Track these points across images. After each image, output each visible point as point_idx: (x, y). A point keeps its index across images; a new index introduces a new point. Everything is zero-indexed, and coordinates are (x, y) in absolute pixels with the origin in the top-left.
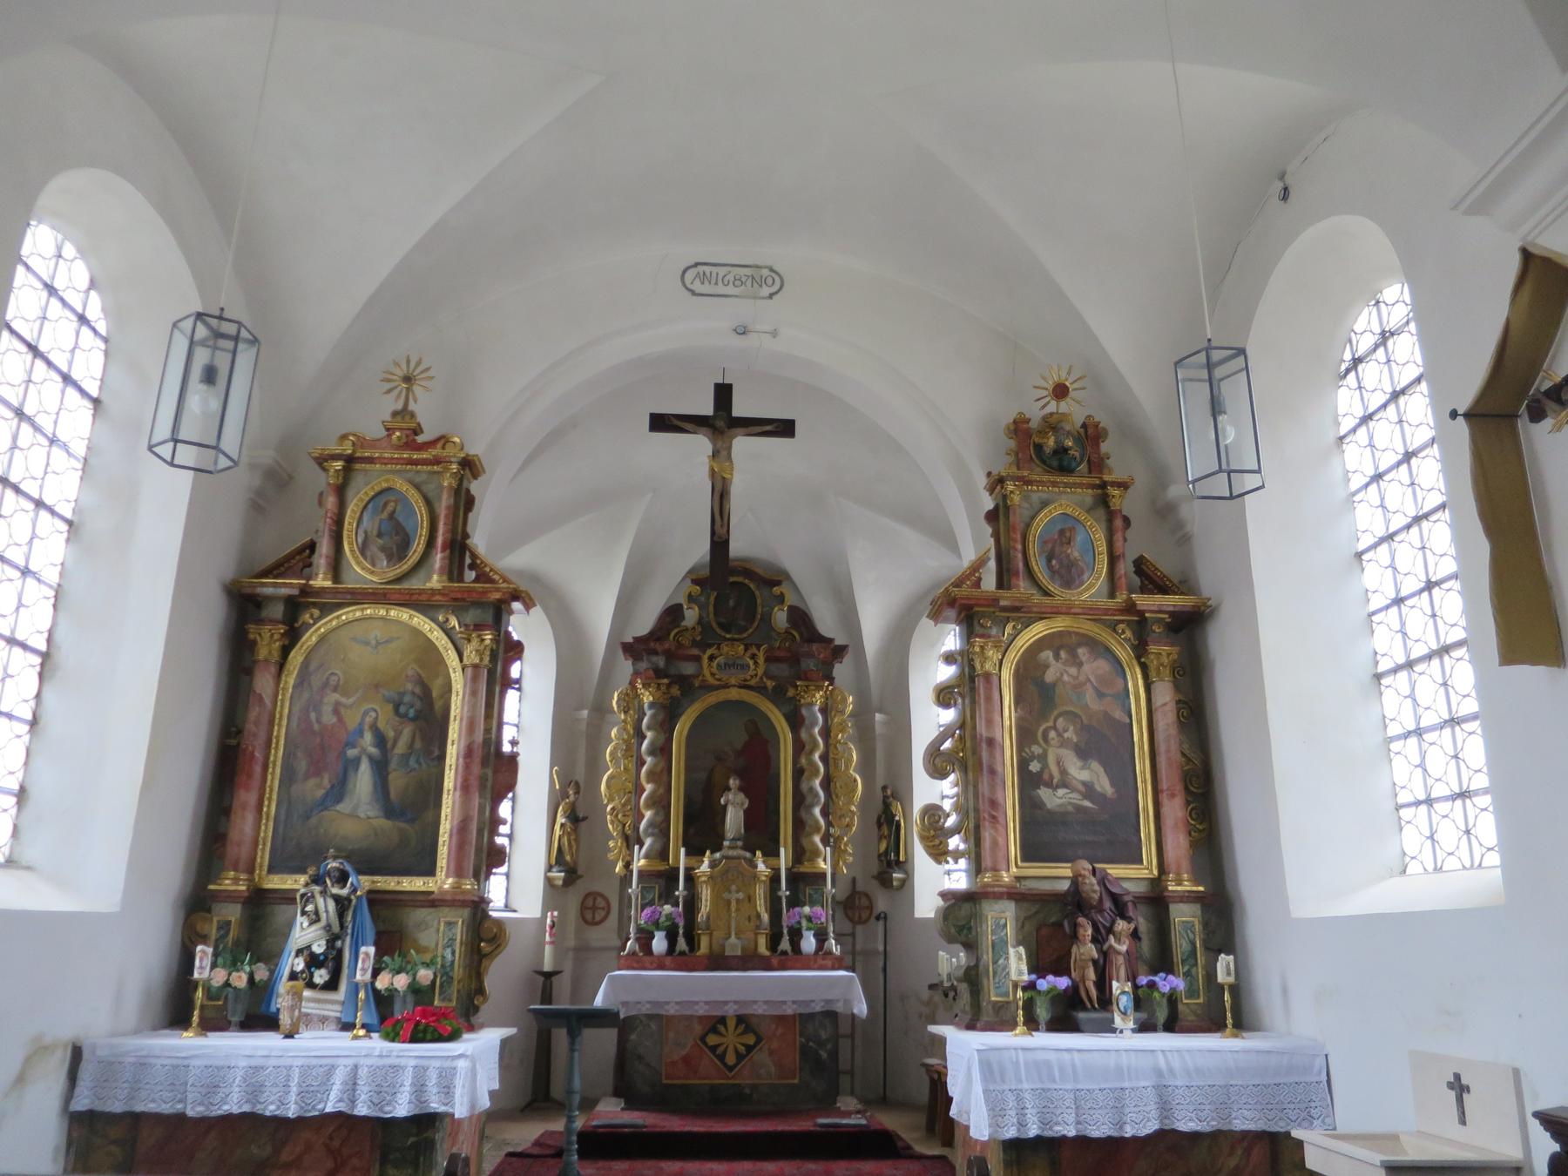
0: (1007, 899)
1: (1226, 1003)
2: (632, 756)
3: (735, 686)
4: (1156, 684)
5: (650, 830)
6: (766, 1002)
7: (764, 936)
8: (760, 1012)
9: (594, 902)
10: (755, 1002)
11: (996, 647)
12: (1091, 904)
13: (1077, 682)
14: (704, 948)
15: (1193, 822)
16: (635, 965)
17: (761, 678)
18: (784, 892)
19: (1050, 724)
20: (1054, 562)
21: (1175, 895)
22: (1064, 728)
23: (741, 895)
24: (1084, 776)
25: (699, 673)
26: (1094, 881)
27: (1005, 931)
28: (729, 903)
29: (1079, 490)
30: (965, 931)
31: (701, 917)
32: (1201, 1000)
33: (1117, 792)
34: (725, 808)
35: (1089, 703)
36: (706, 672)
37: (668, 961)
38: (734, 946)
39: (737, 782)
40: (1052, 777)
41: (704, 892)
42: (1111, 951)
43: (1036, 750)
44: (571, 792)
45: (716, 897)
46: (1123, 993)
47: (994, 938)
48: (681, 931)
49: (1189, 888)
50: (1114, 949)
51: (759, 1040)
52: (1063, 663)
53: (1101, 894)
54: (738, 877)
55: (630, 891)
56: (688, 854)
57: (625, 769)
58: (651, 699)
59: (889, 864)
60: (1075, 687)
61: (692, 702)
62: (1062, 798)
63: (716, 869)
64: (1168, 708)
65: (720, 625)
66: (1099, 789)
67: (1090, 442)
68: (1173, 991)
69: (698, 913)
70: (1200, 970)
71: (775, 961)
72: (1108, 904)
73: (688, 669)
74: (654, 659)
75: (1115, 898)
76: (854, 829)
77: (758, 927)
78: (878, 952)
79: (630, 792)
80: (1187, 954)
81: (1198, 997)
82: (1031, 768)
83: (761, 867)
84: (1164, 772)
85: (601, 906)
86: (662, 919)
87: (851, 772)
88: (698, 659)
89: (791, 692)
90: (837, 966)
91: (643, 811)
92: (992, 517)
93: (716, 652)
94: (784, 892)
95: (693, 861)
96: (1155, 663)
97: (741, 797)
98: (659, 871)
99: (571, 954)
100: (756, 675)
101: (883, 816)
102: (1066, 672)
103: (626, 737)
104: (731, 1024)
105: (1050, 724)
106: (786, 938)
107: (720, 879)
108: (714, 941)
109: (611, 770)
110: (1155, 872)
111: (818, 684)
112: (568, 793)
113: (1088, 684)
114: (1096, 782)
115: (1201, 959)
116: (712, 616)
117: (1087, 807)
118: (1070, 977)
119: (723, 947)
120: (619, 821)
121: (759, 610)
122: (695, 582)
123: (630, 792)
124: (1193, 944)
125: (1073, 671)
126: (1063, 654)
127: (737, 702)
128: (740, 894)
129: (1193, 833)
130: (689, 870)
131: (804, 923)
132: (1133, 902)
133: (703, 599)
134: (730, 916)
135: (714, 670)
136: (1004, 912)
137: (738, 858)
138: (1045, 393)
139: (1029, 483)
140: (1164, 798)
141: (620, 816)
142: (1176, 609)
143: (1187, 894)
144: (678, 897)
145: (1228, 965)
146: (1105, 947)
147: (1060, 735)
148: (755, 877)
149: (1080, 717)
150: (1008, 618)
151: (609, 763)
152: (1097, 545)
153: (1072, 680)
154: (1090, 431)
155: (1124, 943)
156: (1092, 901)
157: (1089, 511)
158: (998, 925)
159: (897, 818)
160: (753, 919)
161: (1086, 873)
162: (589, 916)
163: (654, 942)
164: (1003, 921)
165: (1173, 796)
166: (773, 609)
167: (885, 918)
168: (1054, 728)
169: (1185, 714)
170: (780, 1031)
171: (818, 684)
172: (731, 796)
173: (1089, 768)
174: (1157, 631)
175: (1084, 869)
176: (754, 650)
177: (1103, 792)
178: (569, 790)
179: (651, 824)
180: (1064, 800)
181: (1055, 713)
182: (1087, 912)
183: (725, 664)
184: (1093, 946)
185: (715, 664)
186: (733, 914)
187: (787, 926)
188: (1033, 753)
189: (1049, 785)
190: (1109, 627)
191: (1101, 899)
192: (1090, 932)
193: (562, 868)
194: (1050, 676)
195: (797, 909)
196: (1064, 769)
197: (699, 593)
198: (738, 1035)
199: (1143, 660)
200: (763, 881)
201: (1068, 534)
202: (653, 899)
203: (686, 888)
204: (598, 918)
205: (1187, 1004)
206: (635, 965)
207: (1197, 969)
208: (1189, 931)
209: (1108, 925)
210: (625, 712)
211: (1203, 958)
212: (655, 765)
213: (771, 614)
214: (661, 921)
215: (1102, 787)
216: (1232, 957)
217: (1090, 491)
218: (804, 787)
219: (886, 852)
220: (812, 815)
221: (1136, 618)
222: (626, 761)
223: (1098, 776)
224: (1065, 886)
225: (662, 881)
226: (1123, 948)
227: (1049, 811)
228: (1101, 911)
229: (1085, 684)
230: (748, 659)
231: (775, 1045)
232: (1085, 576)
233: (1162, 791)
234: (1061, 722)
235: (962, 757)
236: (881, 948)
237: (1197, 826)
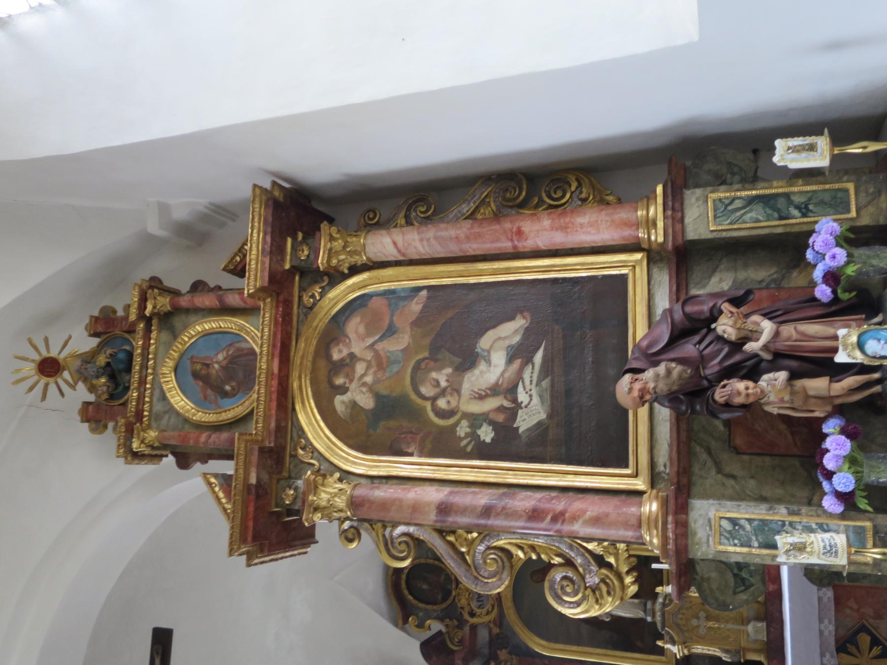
0: (687, 514)
1: (869, 150)
4: (372, 256)
6: (821, 621)
8: (832, 628)
10: (821, 632)
11: (316, 487)
12: (691, 377)
13: (373, 363)
15: (568, 196)
19: (428, 405)
20: (228, 388)
21: (670, 231)
22: (435, 386)
24: (499, 359)
25: (487, 625)
26: (649, 374)
27: (742, 522)
29: (152, 348)
30: (744, 574)
32: (851, 186)
33: (522, 312)
35: (401, 347)
36: (486, 619)
38: (756, 631)
40: (501, 409)
42: (772, 347)
43: (463, 429)
46: (860, 346)
47: (756, 544)
49: (660, 209)
50: (769, 342)
51: (863, 629)
52: (351, 381)
53: (672, 360)
54: (683, 614)
60: (380, 366)
61: (514, 633)
62: (531, 396)
63: (676, 638)
64: (399, 239)
65: (444, 600)
66: (517, 339)
67: (110, 330)
68: (844, 241)
70: (796, 189)
72: (689, 349)
73: (483, 635)
75: (678, 335)
80: (769, 211)
81: (847, 191)
82: (488, 440)
84: (488, 246)
88: (474, 628)
92: (184, 462)
96: (342, 257)
102: (363, 376)
105: (428, 405)
110: (638, 256)
113: (379, 346)
114: (507, 343)
115: (777, 188)
116: (435, 607)
117: (544, 357)
118: (823, 420)
122: (405, 621)
124: (751, 201)
125: (360, 368)
126: (339, 381)
129: (583, 196)
132: (684, 303)
133: (421, 614)
135: (484, 611)
136: (709, 521)
138: (53, 388)
139: (139, 415)
140: (529, 244)
142: (269, 229)
143: (669, 213)
145: (795, 150)
146: (766, 356)
147: (443, 393)
149: (419, 363)
150: (291, 456)
152: (190, 338)
153: (371, 371)
154: (100, 329)
155: (758, 324)
156: (685, 375)
157: (175, 336)
158: (732, 536)
161: (637, 386)
164: (726, 525)
165: (519, 232)
168: (434, 399)
169: (423, 209)
170: (852, 603)
173: (489, 352)
174: (306, 253)
175: (631, 390)
177: (522, 332)
180: (534, 392)
181: (413, 396)
182: (705, 383)
183: (478, 601)
184: (765, 377)
185: (478, 611)
188: (467, 435)
189: (512, 413)
190: (306, 315)
191: (680, 361)
192: (741, 385)
194: (366, 402)
196: (490, 389)
198: (861, 654)
199: (346, 271)
201: (198, 367)
205: (858, 211)
207: (794, 193)
208: (730, 208)
209: (726, 350)
211: (775, 184)
215: (516, 331)
216: (778, 143)
217: (154, 335)
221: (297, 278)
223: (500, 338)
224: (664, 413)
226: (767, 327)
227: (550, 416)
228: (703, 360)
229: (377, 355)
231: (869, 611)
232: (243, 345)
233: (515, 247)
234: (427, 390)
235: (480, 534)
237: (573, 189)
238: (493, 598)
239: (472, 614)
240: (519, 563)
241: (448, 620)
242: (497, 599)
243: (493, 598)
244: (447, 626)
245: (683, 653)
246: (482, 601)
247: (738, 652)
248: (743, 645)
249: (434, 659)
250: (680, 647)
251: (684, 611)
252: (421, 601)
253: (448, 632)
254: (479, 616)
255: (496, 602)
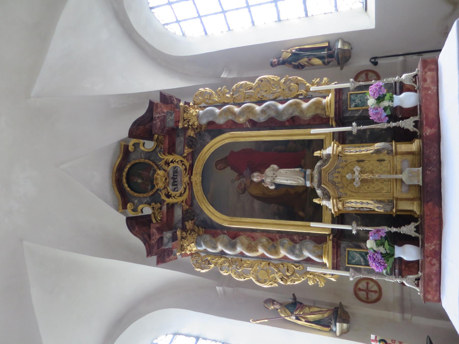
2: (241, 260)
3: (190, 178)
5: (297, 252)
7: (398, 146)
9: (363, 290)
14: (415, 207)
16: (435, 282)
17: (184, 157)
18: (354, 128)
23: (357, 169)
28: (363, 181)
31: (378, 209)
34: (278, 186)
36: (180, 199)
37: (430, 247)
39: (255, 174)
41: (354, 205)
44: (272, 307)
45: (357, 193)
48: (394, 230)
54: (339, 172)
55: (351, 279)
56: (320, 220)
57: (251, 267)
58: (193, 244)
59: (330, 56)
63: (331, 193)
69: (374, 211)
71: (428, 132)
73: (178, 213)
74: (165, 240)
76: (299, 78)
77: (390, 152)
78: (405, 61)
79: (269, 264)
83: (328, 151)
85: (365, 285)
86: (382, 250)
87: (254, 84)
88: (171, 207)
89: (191, 133)
90: (433, 66)
91: (281, 256)
93: (164, 192)
94: (354, 128)
95: (326, 216)
97: (268, 171)
98: (333, 247)
99: (407, 316)
100: (182, 161)
101: (293, 63)
103: (227, 264)
104: (278, 238)
106: (403, 124)
107: (341, 190)
108: (405, 196)
109: (251, 278)
111: (182, 111)
112: (272, 310)
116: (145, 195)
119: (410, 186)
120: (292, 275)
121: (142, 160)
123: (269, 264)
127: (203, 176)
128: (355, 169)
130: (334, 221)
131: (386, 103)
134: (377, 180)
135: (178, 193)
137: (320, 173)
141: (288, 274)
144: (358, 231)
148: (338, 156)
151: (246, 279)
159: (294, 51)
160: (381, 156)
162: (374, 296)
163: (406, 258)
166: (143, 151)
167: (375, 58)
171: (182, 111)
172: (268, 180)
176: (162, 163)
178: (270, 309)
179: (292, 251)
183: (173, 185)
185: (173, 193)
186: (377, 176)
187: (388, 122)
193: (333, 322)
195: (371, 113)
197: (132, 204)
200: (342, 148)
202: (360, 254)
203: (349, 224)
204: (375, 288)
206: (435, 282)
210: (209, 263)
212: (242, 244)
213: (146, 152)
214: (384, 252)
218: (262, 119)
219: (321, 58)
220: (284, 109)
222: (245, 265)
225: (343, 244)
230: (170, 167)
236: (401, 58)
238: (185, 183)
239: (168, 196)
240: (206, 155)
241: (154, 204)
242: (188, 184)
243: (185, 183)
244: (153, 208)
245: (338, 209)
246: (177, 185)
247: (391, 202)
248: (395, 195)
249: (137, 229)
250: (335, 200)
251: (340, 170)
252: (136, 192)
253: (154, 213)
254: (174, 197)
255: (187, 186)
